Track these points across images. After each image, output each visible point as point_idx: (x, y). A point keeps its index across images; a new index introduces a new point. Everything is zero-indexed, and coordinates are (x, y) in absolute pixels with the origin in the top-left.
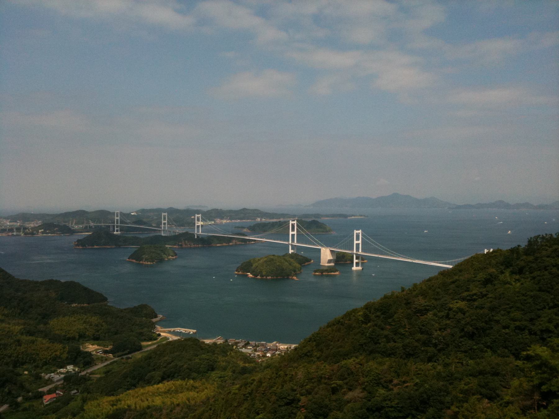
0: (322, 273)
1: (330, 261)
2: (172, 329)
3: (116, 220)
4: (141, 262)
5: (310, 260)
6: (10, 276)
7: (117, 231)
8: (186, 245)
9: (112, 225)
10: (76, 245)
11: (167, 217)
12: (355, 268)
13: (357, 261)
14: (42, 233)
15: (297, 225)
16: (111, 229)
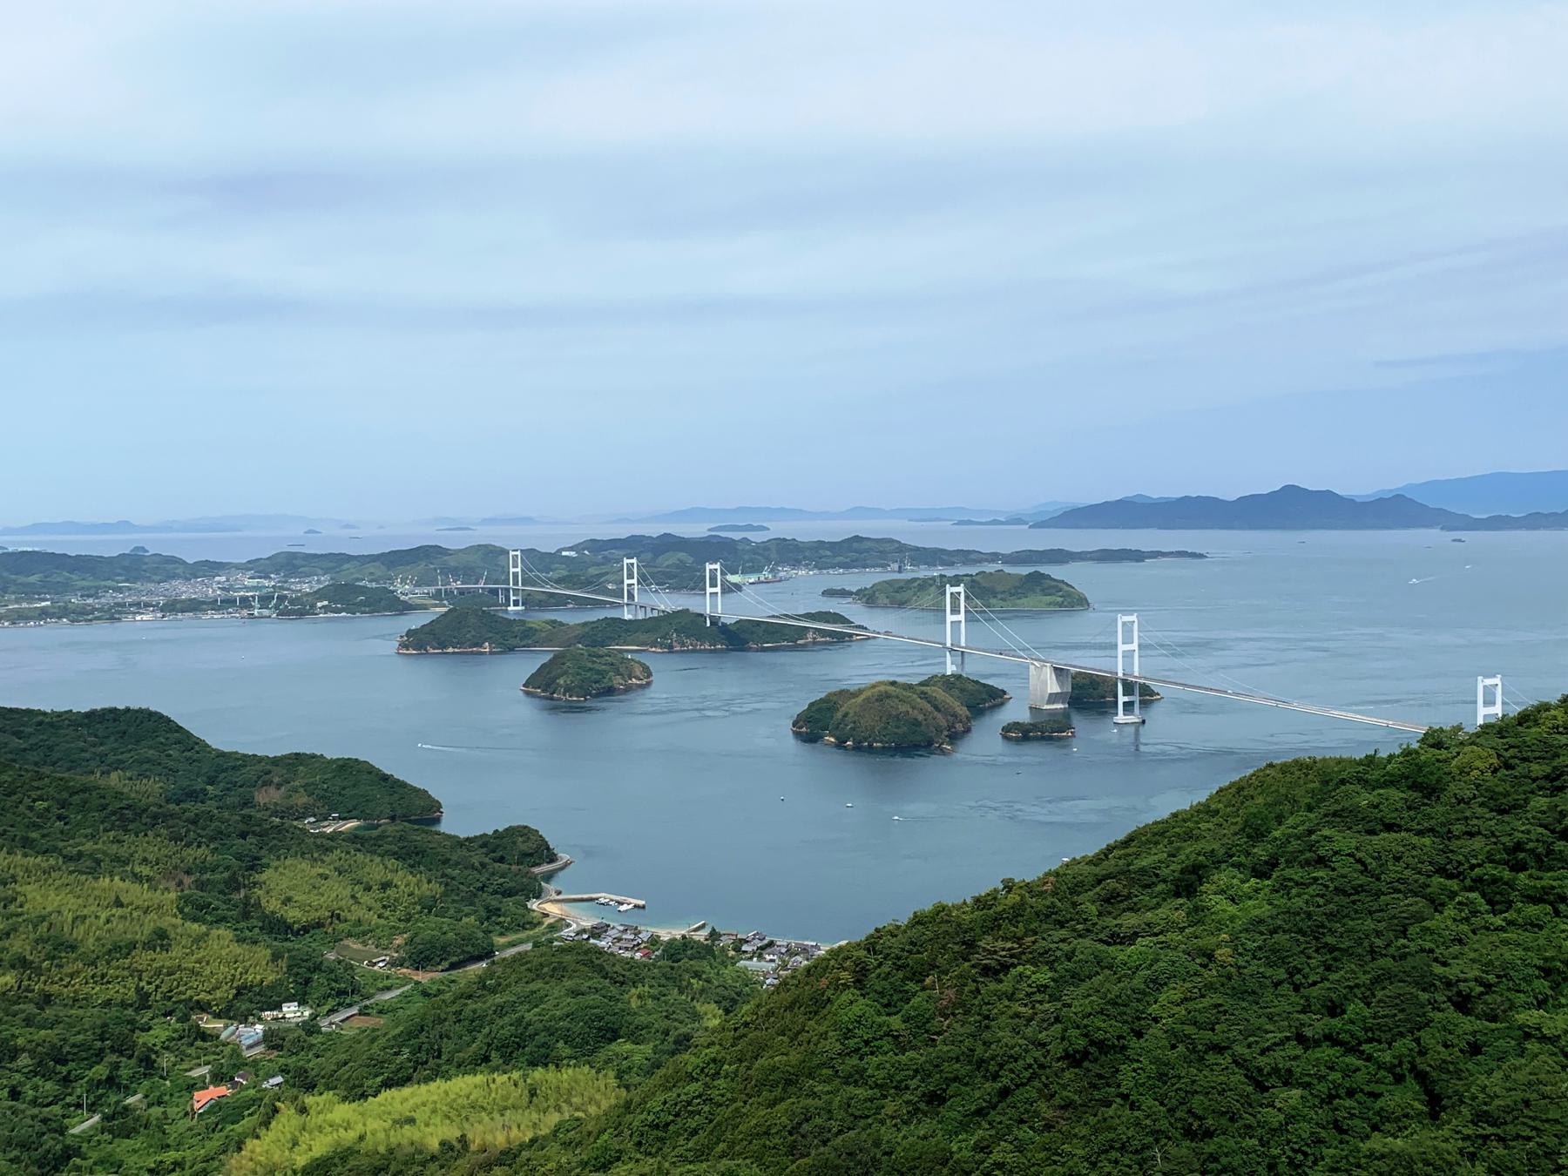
1: (1053, 698)
6: (197, 744)
7: (516, 603)
8: (683, 645)
9: (502, 589)
13: (1126, 699)
15: (967, 597)
16: (501, 599)
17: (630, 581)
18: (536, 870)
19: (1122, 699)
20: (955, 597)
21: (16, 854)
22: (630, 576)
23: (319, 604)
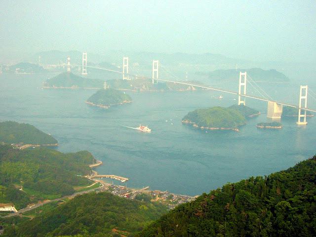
0: (265, 126)
1: (277, 114)
2: (107, 176)
3: (153, 73)
4: (98, 105)
5: (259, 112)
7: (85, 72)
10: (46, 85)
11: (127, 62)
12: (299, 123)
14: (19, 71)
17: (126, 66)
18: (91, 166)
19: (300, 116)
20: (243, 77)
21: (94, 174)
22: (126, 64)
23: (17, 69)
